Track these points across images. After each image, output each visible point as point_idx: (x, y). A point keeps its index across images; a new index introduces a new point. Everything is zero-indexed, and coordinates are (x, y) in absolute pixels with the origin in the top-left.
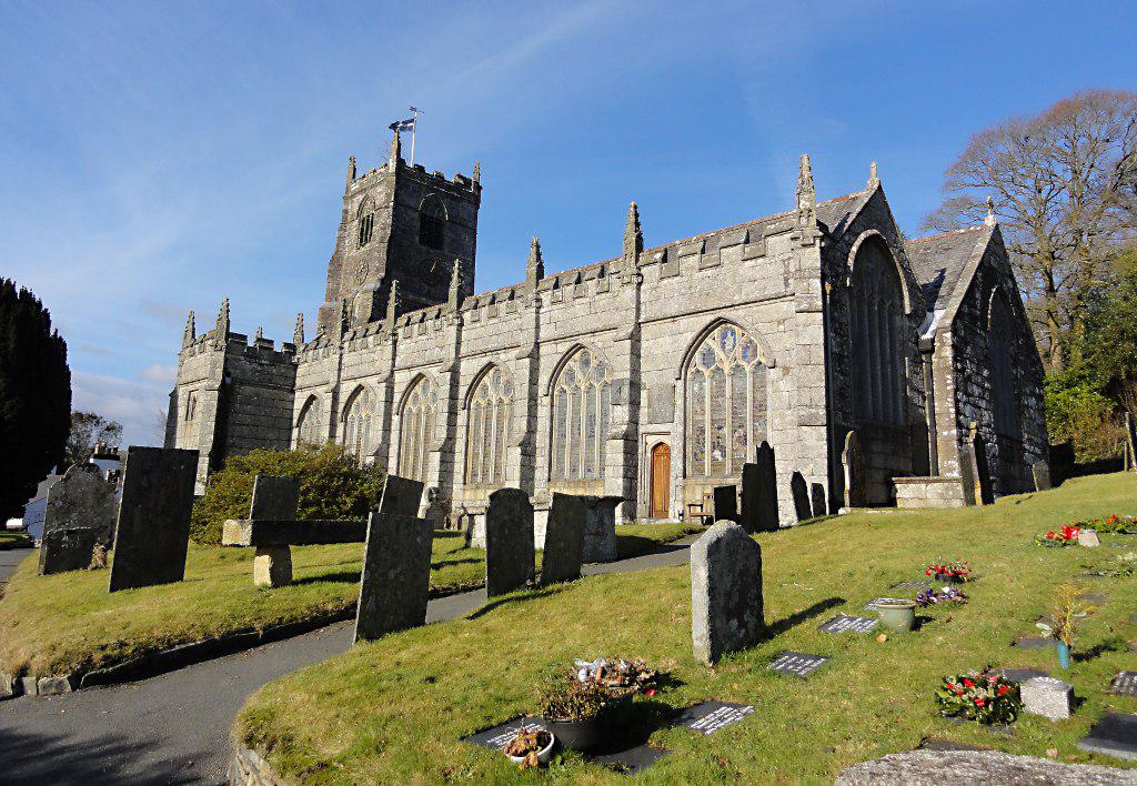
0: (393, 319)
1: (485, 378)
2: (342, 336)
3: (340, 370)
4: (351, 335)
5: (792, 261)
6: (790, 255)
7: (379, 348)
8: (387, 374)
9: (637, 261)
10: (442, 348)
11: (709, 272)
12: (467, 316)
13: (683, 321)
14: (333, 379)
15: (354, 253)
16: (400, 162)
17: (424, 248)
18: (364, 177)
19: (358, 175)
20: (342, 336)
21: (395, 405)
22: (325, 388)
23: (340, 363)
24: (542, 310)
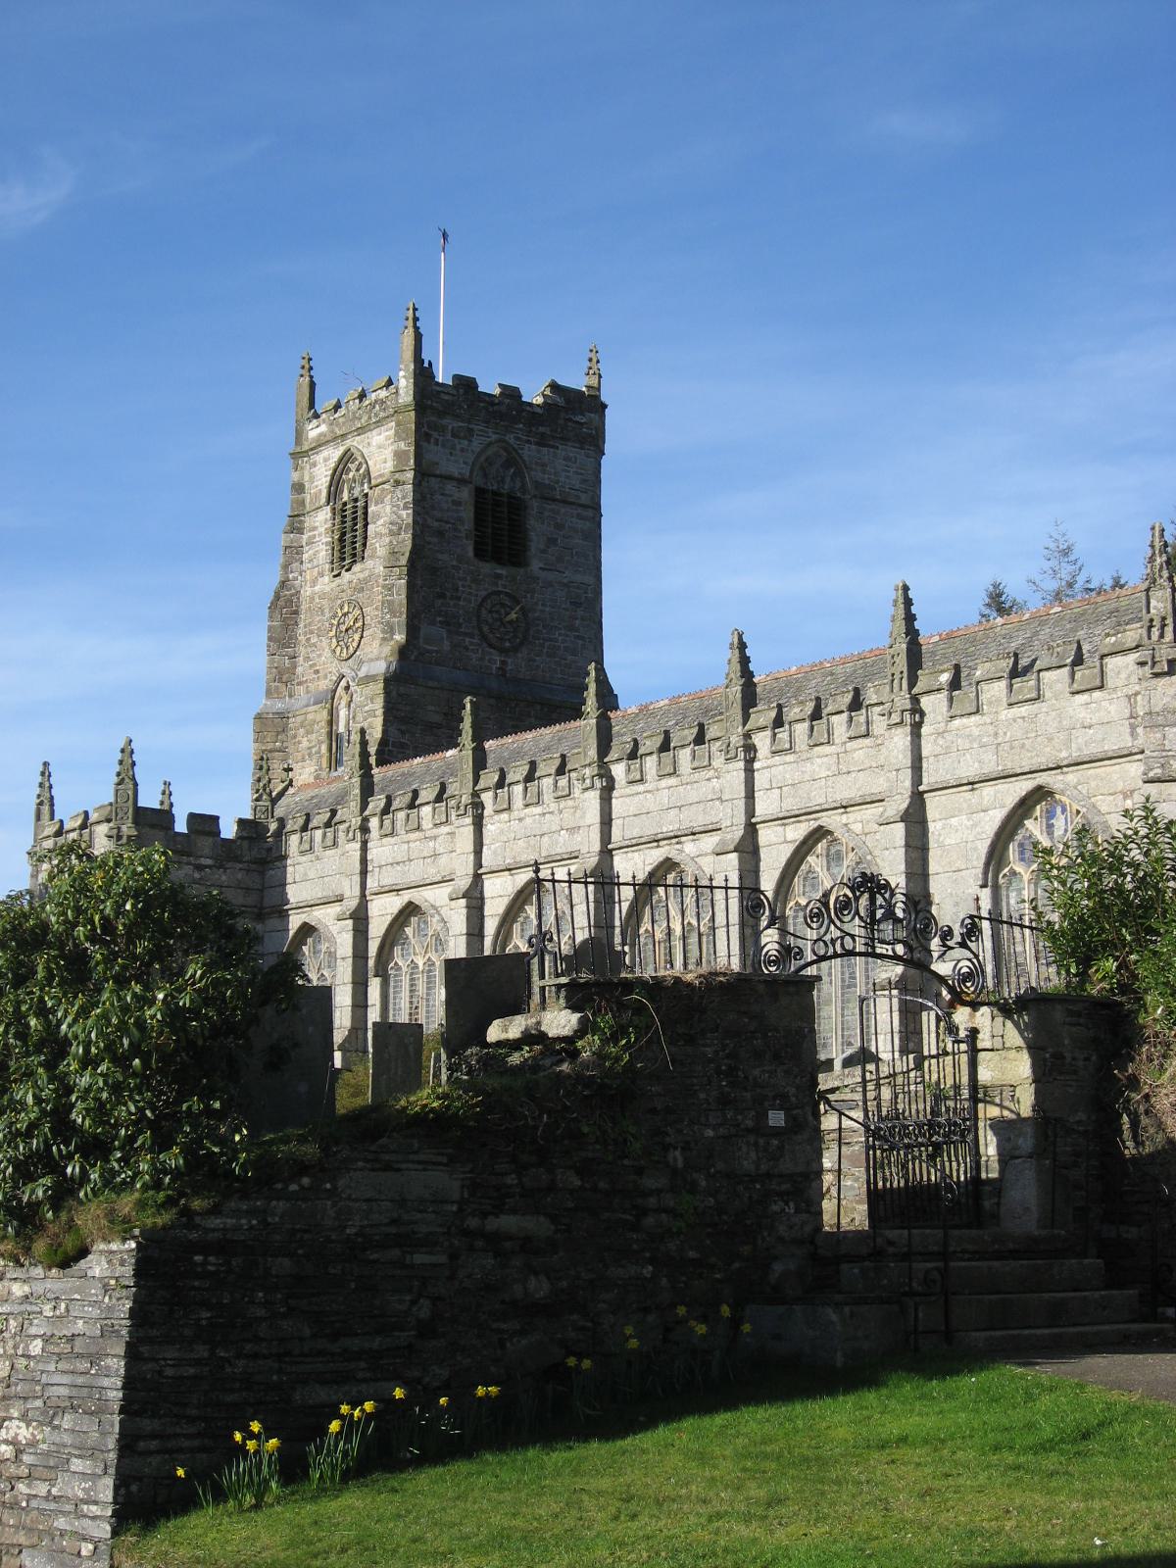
0: (470, 776)
1: (810, 859)
2: (364, 805)
3: (364, 873)
4: (382, 804)
5: (1139, 697)
6: (1137, 688)
7: (445, 829)
8: (464, 883)
9: (911, 685)
10: (572, 830)
11: (1024, 710)
12: (618, 770)
13: (987, 791)
14: (351, 891)
15: (326, 584)
16: (423, 374)
17: (487, 568)
18: (337, 407)
19: (324, 403)
20: (364, 805)
21: (371, 963)
22: (334, 910)
23: (364, 861)
24: (757, 765)
